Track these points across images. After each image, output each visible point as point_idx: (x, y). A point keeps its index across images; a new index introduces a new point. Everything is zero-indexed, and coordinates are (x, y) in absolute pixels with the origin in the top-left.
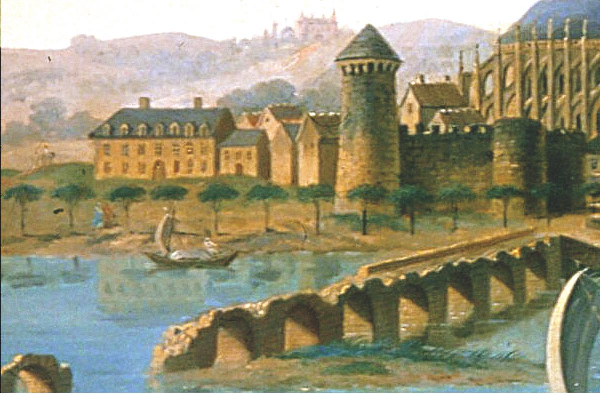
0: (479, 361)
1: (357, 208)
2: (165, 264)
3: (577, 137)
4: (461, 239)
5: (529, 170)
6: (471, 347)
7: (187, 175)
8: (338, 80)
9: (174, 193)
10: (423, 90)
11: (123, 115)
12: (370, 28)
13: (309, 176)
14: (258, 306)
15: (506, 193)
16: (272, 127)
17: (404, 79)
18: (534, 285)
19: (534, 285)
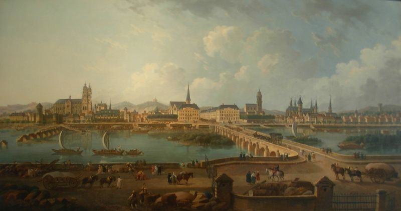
0: (52, 140)
1: (38, 123)
2: (17, 130)
3: (62, 115)
4: (49, 127)
5: (57, 119)
6: (51, 139)
7: (293, 127)
8: (36, 109)
9: (18, 122)
10: (45, 110)
11: (13, 113)
12: (171, 102)
13: (33, 120)
14: (28, 135)
15: (54, 122)
16: (29, 115)
17: (43, 109)
18: (57, 132)
19: (57, 132)
